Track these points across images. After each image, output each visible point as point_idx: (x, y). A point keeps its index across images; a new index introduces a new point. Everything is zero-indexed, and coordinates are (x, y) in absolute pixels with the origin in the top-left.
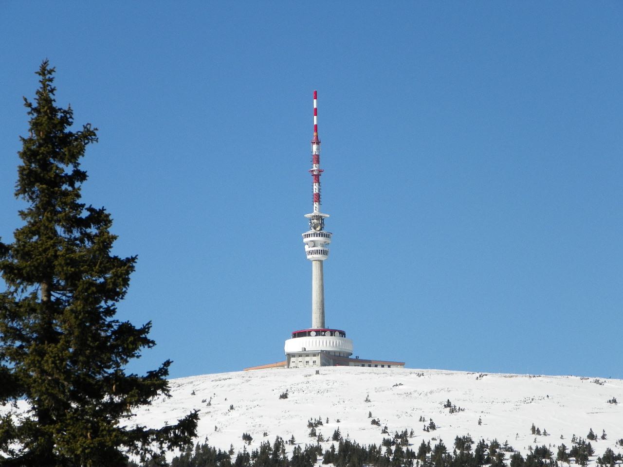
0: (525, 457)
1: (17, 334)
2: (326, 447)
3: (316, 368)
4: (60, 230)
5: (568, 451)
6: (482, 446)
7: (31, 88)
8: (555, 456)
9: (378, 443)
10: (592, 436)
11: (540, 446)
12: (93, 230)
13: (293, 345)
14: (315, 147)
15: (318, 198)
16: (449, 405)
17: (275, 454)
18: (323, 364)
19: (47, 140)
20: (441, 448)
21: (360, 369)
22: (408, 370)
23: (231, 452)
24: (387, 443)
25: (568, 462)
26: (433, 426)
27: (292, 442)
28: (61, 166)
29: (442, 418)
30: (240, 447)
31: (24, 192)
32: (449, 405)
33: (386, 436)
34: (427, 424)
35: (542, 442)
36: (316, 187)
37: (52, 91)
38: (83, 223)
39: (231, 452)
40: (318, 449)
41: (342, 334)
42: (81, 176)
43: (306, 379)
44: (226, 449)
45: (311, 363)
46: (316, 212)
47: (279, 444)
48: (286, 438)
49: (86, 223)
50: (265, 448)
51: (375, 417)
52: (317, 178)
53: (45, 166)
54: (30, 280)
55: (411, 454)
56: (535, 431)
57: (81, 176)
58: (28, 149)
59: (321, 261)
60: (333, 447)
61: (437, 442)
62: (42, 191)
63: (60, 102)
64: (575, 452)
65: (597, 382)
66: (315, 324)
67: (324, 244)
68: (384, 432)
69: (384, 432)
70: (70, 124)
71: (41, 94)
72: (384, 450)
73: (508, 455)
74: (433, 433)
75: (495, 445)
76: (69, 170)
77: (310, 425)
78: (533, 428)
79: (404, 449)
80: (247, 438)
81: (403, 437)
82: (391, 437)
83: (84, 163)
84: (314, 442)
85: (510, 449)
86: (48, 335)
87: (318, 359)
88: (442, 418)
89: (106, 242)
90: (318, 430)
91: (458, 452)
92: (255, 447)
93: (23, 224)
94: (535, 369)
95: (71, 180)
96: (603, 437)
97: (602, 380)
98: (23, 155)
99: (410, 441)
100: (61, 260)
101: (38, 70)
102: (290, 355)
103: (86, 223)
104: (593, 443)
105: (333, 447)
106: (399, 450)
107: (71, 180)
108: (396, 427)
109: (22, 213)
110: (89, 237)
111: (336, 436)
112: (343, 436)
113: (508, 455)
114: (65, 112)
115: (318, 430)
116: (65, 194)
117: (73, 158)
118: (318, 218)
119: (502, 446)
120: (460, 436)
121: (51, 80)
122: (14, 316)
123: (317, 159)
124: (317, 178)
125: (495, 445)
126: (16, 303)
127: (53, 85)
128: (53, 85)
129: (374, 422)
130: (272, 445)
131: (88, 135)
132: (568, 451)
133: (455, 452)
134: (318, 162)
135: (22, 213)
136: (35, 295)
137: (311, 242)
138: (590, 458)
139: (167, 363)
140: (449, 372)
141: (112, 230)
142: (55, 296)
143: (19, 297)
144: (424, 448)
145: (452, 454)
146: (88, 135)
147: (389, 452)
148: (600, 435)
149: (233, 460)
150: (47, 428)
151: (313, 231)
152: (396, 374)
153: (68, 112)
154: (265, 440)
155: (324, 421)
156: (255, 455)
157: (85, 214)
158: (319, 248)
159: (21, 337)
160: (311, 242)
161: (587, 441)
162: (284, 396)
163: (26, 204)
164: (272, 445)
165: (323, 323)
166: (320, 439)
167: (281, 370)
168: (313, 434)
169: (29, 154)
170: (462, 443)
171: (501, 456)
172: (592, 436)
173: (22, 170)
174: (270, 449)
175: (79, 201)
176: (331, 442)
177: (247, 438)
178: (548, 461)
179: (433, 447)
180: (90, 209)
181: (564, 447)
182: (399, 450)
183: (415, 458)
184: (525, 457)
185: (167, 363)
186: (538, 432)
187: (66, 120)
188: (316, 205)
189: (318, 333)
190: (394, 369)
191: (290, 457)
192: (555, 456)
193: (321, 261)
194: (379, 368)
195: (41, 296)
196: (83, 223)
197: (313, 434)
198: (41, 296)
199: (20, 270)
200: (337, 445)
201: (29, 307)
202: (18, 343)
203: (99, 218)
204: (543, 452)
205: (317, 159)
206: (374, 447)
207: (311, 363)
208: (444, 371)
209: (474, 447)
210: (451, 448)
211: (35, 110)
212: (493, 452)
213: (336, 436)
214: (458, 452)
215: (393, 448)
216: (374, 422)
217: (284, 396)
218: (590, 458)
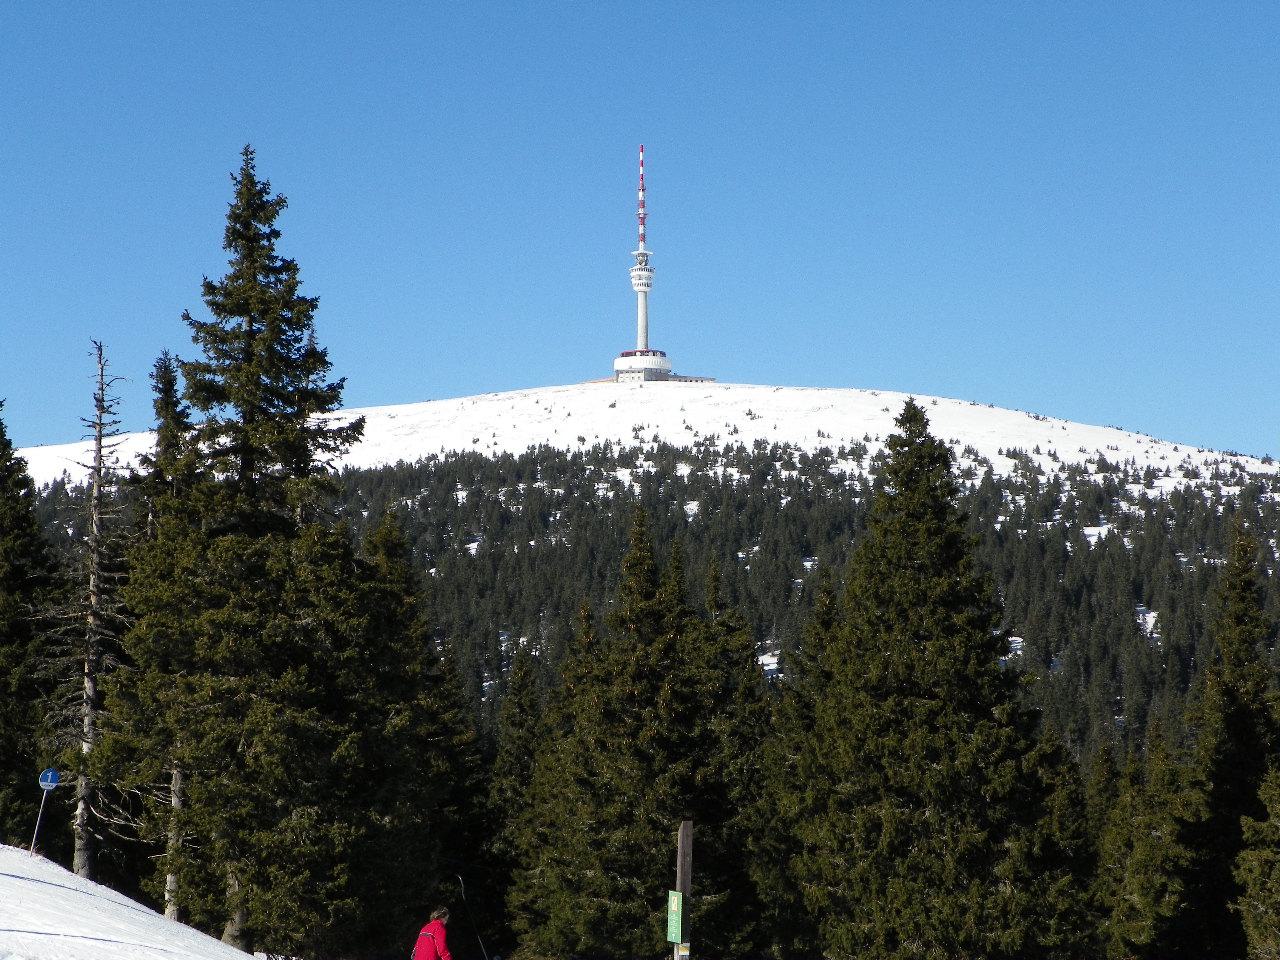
0: (811, 456)
1: (226, 355)
2: (646, 447)
3: (640, 383)
4: (260, 277)
5: (846, 451)
6: (776, 447)
7: (237, 164)
8: (835, 455)
9: (690, 444)
10: (867, 439)
11: (824, 446)
12: (284, 276)
13: (621, 363)
14: (641, 193)
15: (643, 238)
16: (750, 413)
17: (605, 454)
18: (646, 380)
19: (249, 205)
20: (742, 449)
21: (677, 383)
22: (718, 385)
23: (568, 451)
24: (698, 444)
25: (847, 460)
26: (736, 431)
27: (619, 443)
28: (260, 226)
29: (743, 423)
30: (575, 447)
31: (230, 246)
32: (750, 413)
33: (697, 439)
34: (732, 429)
35: (825, 443)
36: (641, 228)
37: (252, 168)
38: (277, 271)
39: (568, 451)
40: (641, 449)
41: (663, 354)
42: (276, 234)
43: (631, 392)
44: (562, 448)
45: (636, 378)
46: (641, 250)
47: (608, 446)
48: (614, 440)
49: (278, 271)
50: (596, 448)
51: (688, 423)
52: (643, 221)
53: (247, 225)
54: (232, 313)
55: (717, 454)
56: (820, 434)
57: (276, 234)
58: (233, 212)
59: (645, 293)
60: (652, 448)
61: (739, 444)
62: (243, 245)
63: (260, 176)
64: (852, 452)
65: (873, 394)
66: (640, 346)
67: (650, 278)
68: (695, 435)
69: (695, 435)
70: (268, 194)
71: (244, 170)
72: (695, 450)
73: (797, 454)
74: (735, 436)
75: (787, 446)
76: (265, 229)
77: (634, 429)
78: (819, 432)
79: (711, 449)
80: (582, 440)
81: (711, 440)
82: (701, 440)
83: (277, 224)
84: (636, 443)
85: (799, 449)
86: (249, 356)
87: (642, 375)
88: (743, 423)
89: (291, 288)
90: (641, 434)
91: (756, 451)
92: (587, 447)
93: (230, 270)
94: (823, 384)
95: (268, 237)
96: (877, 440)
97: (877, 392)
98: (230, 217)
99: (717, 443)
100: (254, 300)
101: (242, 151)
102: (619, 372)
103: (278, 271)
104: (868, 445)
105: (652, 448)
106: (707, 450)
107: (268, 237)
108: (705, 432)
109: (230, 262)
110: (281, 281)
111: (655, 439)
112: (662, 439)
113: (797, 454)
114: (263, 184)
115: (641, 434)
116: (263, 247)
117: (268, 220)
118: (644, 255)
119: (792, 447)
120: (758, 438)
121: (252, 159)
122: (223, 341)
123: (643, 204)
124: (643, 221)
125: (787, 446)
126: (225, 331)
127: (254, 163)
128: (254, 163)
129: (687, 427)
130: (602, 446)
131: (281, 202)
132: (846, 451)
133: (753, 452)
134: (644, 207)
135: (230, 262)
136: (240, 325)
137: (637, 277)
138: (864, 456)
139: (343, 380)
140: (560, 388)
141: (299, 277)
142: (256, 326)
143: (228, 328)
144: (728, 449)
145: (751, 453)
146: (281, 202)
147: (699, 451)
148: (873, 439)
149: (569, 457)
150: (248, 428)
151: (639, 266)
152: (706, 387)
153: (266, 185)
154: (596, 441)
155: (646, 427)
156: (588, 453)
157: (278, 264)
158: (644, 281)
159: (230, 357)
160: (637, 277)
161: (863, 443)
162: (613, 406)
163: (232, 255)
164: (602, 446)
165: (647, 345)
166: (642, 441)
167: (611, 384)
168: (636, 437)
169: (234, 217)
170: (759, 444)
171: (791, 454)
172: (867, 439)
173: (228, 229)
174: (600, 449)
175: (274, 254)
176: (652, 444)
177: (582, 440)
178: (830, 459)
179: (735, 448)
180: (283, 260)
181: (843, 448)
182: (707, 450)
183: (720, 456)
184: (811, 456)
185: (343, 380)
186: (823, 437)
187: (265, 190)
188: (641, 244)
189: (643, 353)
190: (706, 383)
191: (616, 455)
192: (835, 455)
193: (645, 293)
194: (694, 383)
195: (245, 327)
196: (277, 271)
197: (636, 437)
198: (245, 327)
199: (224, 306)
200: (656, 446)
201: (235, 334)
202: (227, 362)
203: (290, 267)
204: (826, 452)
205: (643, 204)
206: (686, 448)
207: (636, 378)
208: (748, 385)
209: (769, 448)
210: (750, 448)
211: (240, 182)
212: (785, 452)
213: (655, 439)
214: (756, 451)
215: (702, 449)
216: (687, 427)
217: (613, 406)
218: (864, 456)
